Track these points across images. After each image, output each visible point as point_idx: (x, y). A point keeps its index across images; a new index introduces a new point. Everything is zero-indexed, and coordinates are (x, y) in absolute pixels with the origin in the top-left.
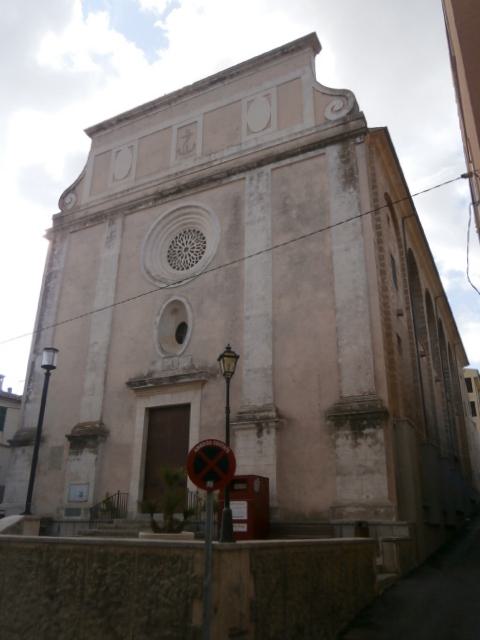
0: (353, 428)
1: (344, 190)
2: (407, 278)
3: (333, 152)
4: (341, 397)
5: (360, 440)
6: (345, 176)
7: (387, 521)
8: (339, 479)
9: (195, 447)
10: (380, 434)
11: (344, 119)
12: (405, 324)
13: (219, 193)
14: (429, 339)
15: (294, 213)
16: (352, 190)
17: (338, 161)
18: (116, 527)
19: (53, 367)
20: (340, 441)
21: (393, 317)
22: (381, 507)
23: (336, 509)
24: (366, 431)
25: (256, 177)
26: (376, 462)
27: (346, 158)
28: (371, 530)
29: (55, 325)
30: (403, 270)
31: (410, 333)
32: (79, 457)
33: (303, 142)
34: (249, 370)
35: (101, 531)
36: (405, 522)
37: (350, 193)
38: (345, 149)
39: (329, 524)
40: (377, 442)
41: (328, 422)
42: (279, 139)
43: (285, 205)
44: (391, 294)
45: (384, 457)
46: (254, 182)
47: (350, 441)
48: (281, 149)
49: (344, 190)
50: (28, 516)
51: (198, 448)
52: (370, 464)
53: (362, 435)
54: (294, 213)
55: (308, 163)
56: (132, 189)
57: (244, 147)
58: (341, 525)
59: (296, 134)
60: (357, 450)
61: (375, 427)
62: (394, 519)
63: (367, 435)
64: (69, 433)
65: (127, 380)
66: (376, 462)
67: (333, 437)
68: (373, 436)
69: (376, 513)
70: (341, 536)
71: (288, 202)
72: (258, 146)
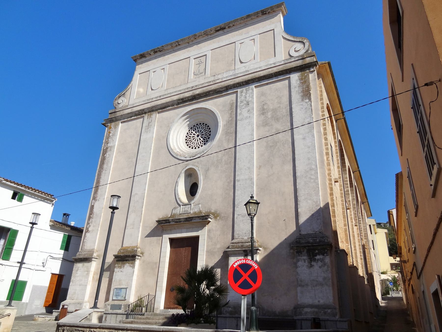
0: (309, 255)
1: (302, 100)
2: (339, 158)
3: (295, 77)
4: (300, 234)
5: (313, 263)
6: (303, 91)
7: (333, 318)
8: (299, 289)
9: (234, 264)
10: (327, 260)
11: (302, 55)
12: (339, 188)
13: (229, 99)
14: (351, 198)
15: (269, 115)
16: (307, 101)
17: (298, 82)
18: (147, 318)
19: (117, 208)
20: (300, 264)
21: (333, 183)
22: (330, 309)
23: (298, 308)
24: (318, 257)
25: (245, 91)
26: (324, 279)
27: (305, 82)
28: (322, 323)
29: (134, 177)
30: (337, 153)
31: (341, 194)
32: (122, 270)
33: (275, 70)
34: (239, 215)
35: (136, 320)
36: (345, 319)
37: (306, 102)
38: (302, 75)
39: (293, 319)
40: (325, 264)
41: (292, 251)
42: (260, 67)
43: (264, 109)
44: (332, 168)
45: (330, 275)
46: (244, 94)
47: (306, 264)
48: (262, 74)
49: (302, 100)
50: (96, 310)
51: (236, 264)
52: (320, 279)
53: (315, 260)
54: (269, 115)
55: (278, 84)
56: (163, 95)
57: (237, 72)
58: (302, 320)
59: (271, 64)
60: (312, 269)
61: (323, 255)
62: (338, 317)
63: (318, 260)
64: (116, 253)
65: (157, 220)
66: (324, 279)
67: (295, 260)
68: (322, 260)
69: (325, 313)
70: (301, 329)
71: (265, 107)
72: (246, 71)
